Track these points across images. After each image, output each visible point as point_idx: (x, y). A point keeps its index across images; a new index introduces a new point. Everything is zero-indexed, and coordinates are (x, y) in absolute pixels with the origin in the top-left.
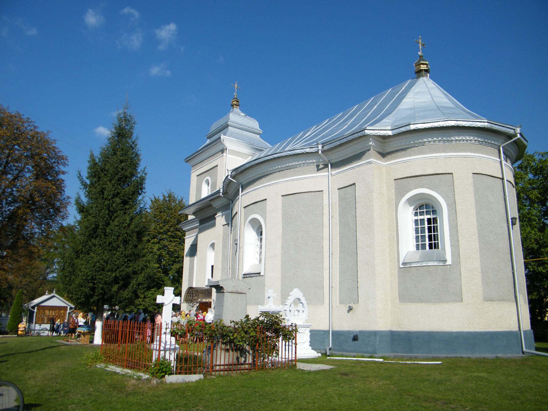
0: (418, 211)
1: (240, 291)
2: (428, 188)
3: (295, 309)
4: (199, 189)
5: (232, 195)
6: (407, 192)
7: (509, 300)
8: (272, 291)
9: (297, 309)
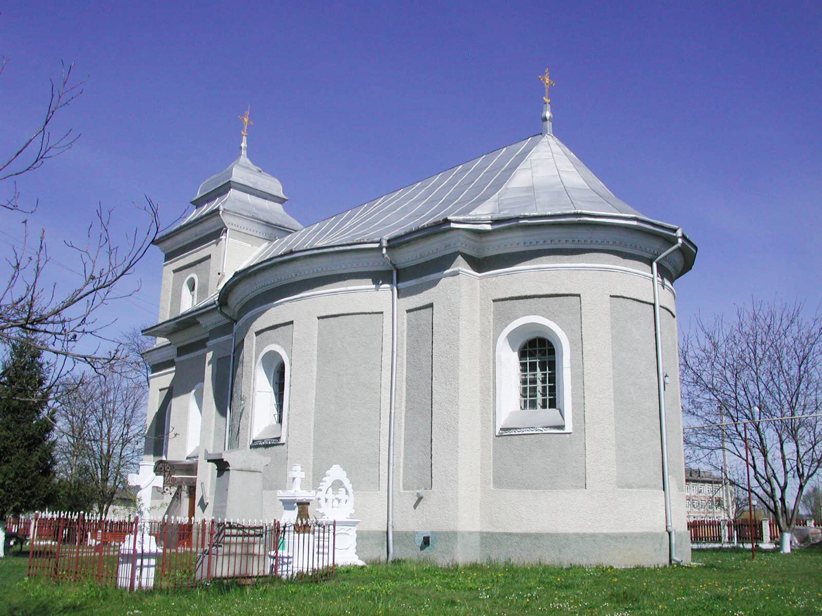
0: (528, 349)
1: (253, 468)
2: (543, 316)
3: (334, 497)
4: (177, 295)
5: (237, 310)
6: (512, 320)
7: (655, 487)
8: (298, 468)
9: (337, 496)
